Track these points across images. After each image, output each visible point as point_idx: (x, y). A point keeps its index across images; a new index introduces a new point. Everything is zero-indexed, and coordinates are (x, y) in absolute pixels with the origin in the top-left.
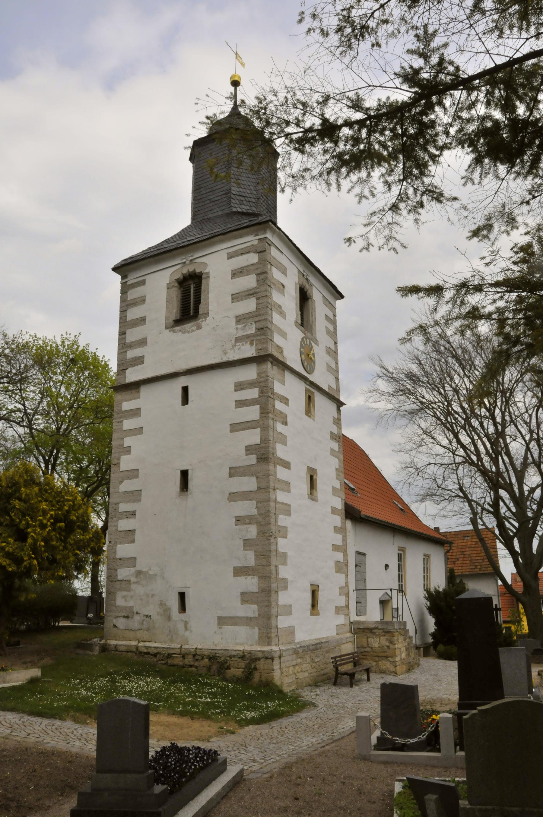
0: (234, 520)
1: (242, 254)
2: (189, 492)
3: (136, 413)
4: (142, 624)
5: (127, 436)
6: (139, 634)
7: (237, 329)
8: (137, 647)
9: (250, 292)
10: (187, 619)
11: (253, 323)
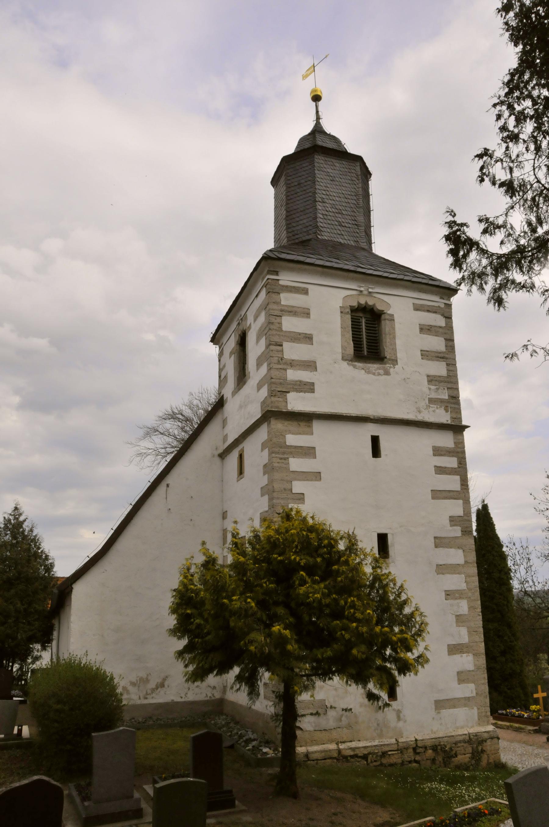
0: (444, 593)
1: (428, 311)
2: (390, 560)
3: (309, 452)
4: (340, 720)
5: (296, 479)
6: (335, 735)
7: (430, 389)
8: (339, 751)
9: (440, 355)
10: (400, 708)
11: (446, 388)
